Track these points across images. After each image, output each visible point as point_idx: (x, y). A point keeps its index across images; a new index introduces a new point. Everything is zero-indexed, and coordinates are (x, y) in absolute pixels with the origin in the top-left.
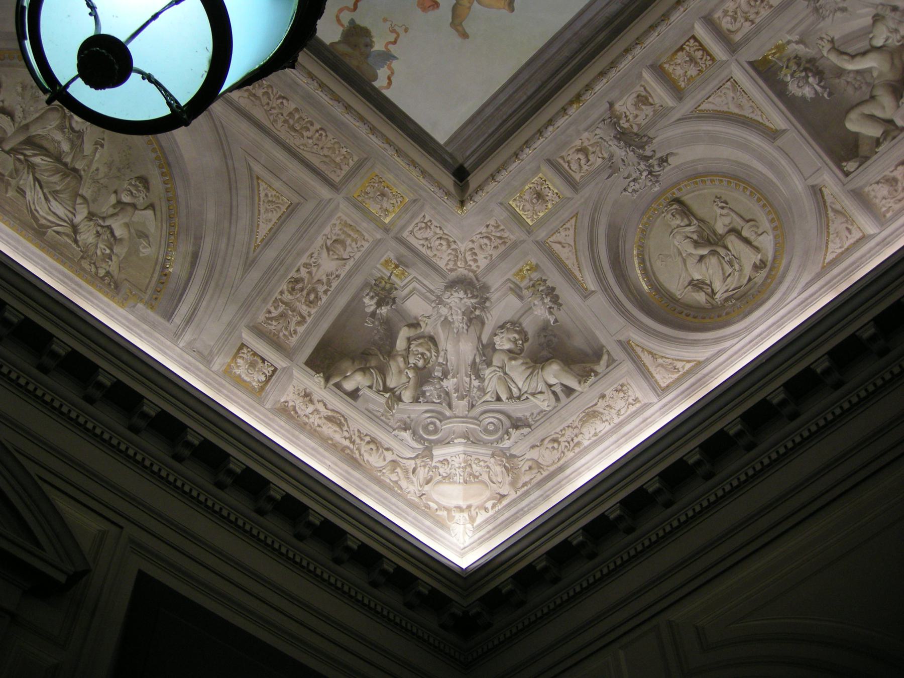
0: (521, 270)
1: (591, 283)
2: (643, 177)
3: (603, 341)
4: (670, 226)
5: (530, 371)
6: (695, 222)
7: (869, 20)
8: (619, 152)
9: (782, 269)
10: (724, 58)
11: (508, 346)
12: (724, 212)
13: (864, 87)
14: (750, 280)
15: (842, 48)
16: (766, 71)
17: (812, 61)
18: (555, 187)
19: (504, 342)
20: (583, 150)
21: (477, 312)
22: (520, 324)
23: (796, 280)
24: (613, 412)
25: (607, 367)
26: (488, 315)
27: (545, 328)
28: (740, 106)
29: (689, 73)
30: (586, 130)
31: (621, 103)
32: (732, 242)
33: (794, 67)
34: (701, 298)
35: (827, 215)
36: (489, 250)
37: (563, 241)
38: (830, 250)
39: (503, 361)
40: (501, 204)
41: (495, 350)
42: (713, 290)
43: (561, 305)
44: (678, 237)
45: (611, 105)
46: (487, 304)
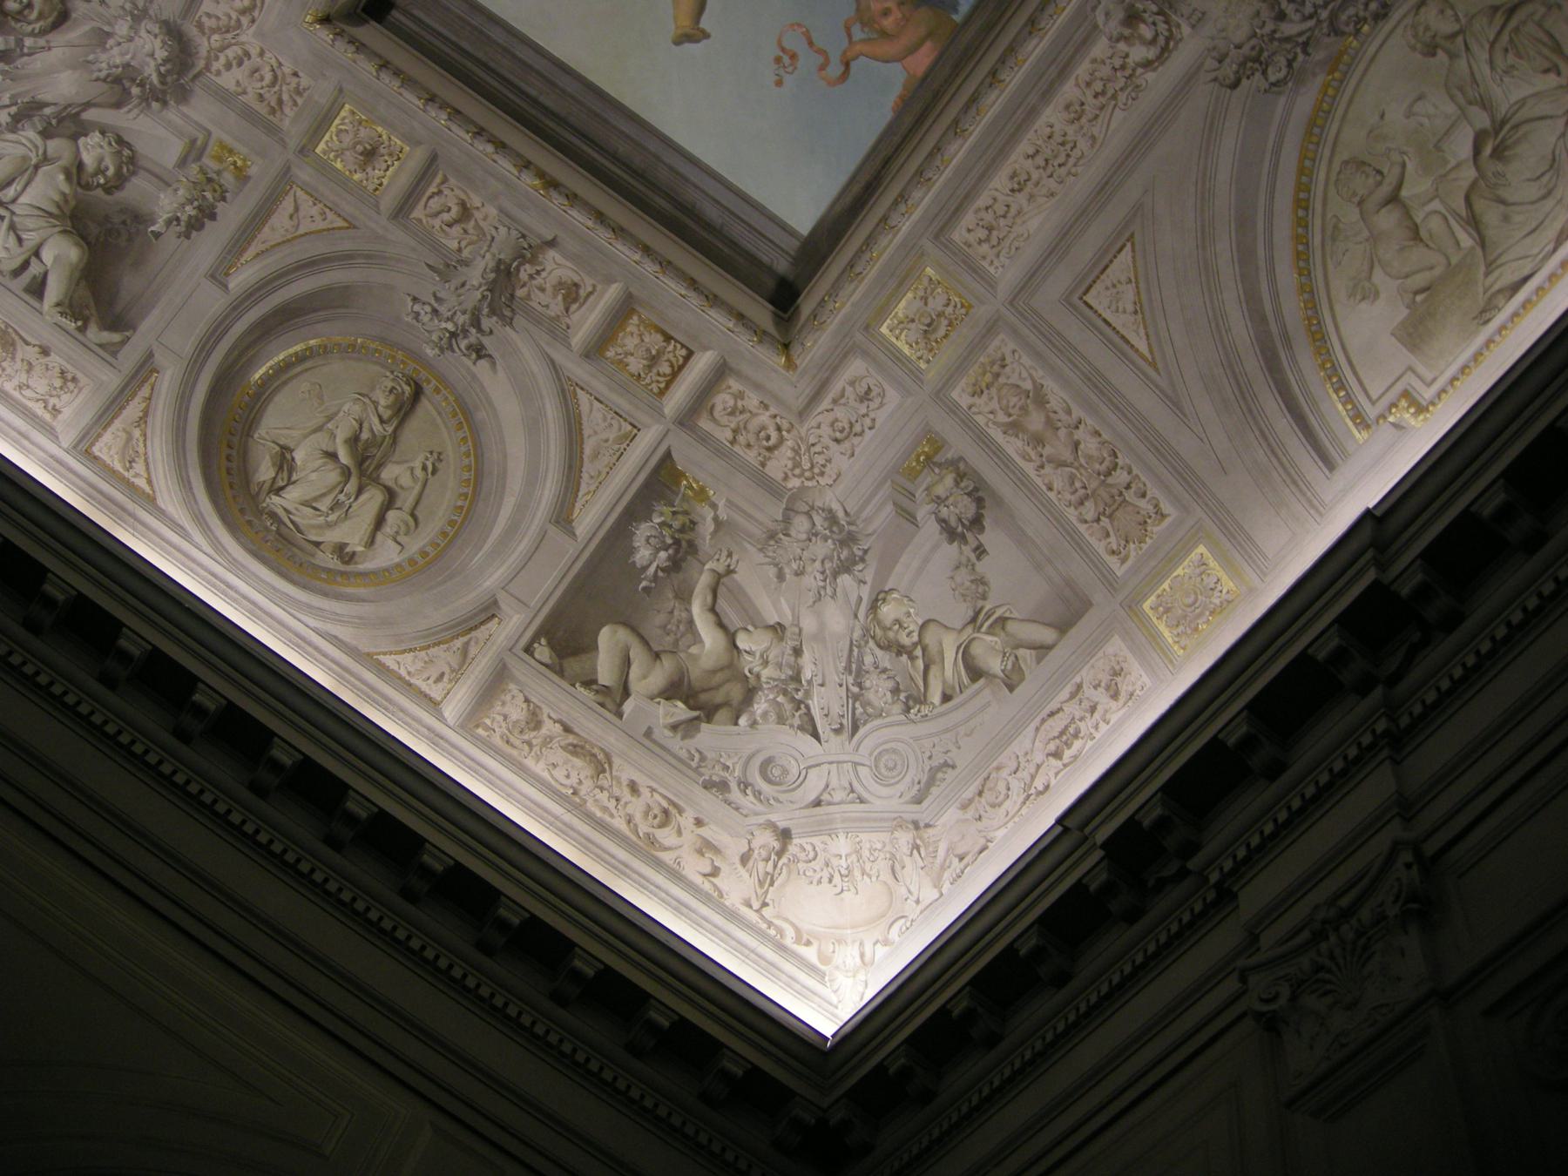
0: (231, 152)
1: (242, 279)
2: (444, 325)
3: (144, 327)
4: (373, 389)
5: (54, 210)
6: (390, 429)
7: (773, 618)
8: (476, 275)
9: (349, 590)
10: (667, 411)
11: (88, 159)
12: (419, 473)
13: (670, 639)
14: (317, 544)
15: (722, 590)
16: (662, 481)
17: (693, 548)
18: (392, 178)
19: (93, 150)
20: (466, 212)
21: (135, 91)
22: (134, 173)
23: (337, 619)
24: (23, 377)
25: (100, 346)
26: (136, 111)
27: (139, 217)
28: (596, 455)
29: (630, 359)
30: (501, 210)
31: (558, 258)
32: (373, 499)
33: (676, 524)
34: (265, 472)
35: (457, 637)
36: (253, 87)
37: (301, 214)
38: (399, 658)
39: (59, 158)
40: (341, 90)
41: (74, 138)
42: (282, 488)
43: (188, 237)
44: (357, 408)
45: (552, 244)
46: (155, 105)
